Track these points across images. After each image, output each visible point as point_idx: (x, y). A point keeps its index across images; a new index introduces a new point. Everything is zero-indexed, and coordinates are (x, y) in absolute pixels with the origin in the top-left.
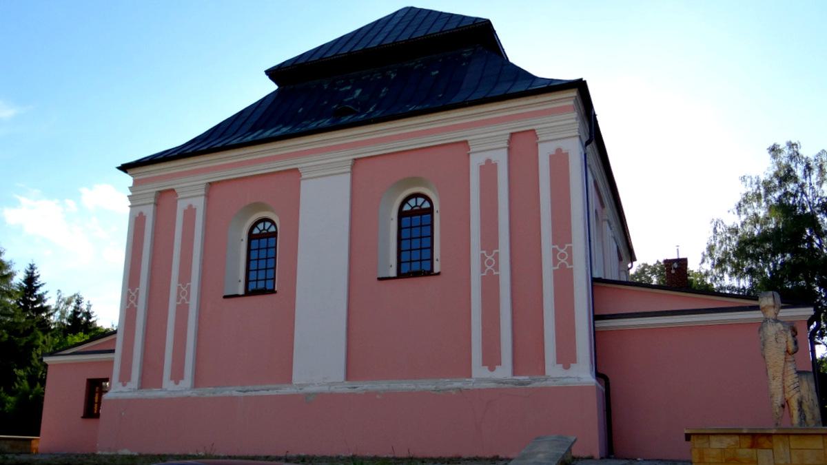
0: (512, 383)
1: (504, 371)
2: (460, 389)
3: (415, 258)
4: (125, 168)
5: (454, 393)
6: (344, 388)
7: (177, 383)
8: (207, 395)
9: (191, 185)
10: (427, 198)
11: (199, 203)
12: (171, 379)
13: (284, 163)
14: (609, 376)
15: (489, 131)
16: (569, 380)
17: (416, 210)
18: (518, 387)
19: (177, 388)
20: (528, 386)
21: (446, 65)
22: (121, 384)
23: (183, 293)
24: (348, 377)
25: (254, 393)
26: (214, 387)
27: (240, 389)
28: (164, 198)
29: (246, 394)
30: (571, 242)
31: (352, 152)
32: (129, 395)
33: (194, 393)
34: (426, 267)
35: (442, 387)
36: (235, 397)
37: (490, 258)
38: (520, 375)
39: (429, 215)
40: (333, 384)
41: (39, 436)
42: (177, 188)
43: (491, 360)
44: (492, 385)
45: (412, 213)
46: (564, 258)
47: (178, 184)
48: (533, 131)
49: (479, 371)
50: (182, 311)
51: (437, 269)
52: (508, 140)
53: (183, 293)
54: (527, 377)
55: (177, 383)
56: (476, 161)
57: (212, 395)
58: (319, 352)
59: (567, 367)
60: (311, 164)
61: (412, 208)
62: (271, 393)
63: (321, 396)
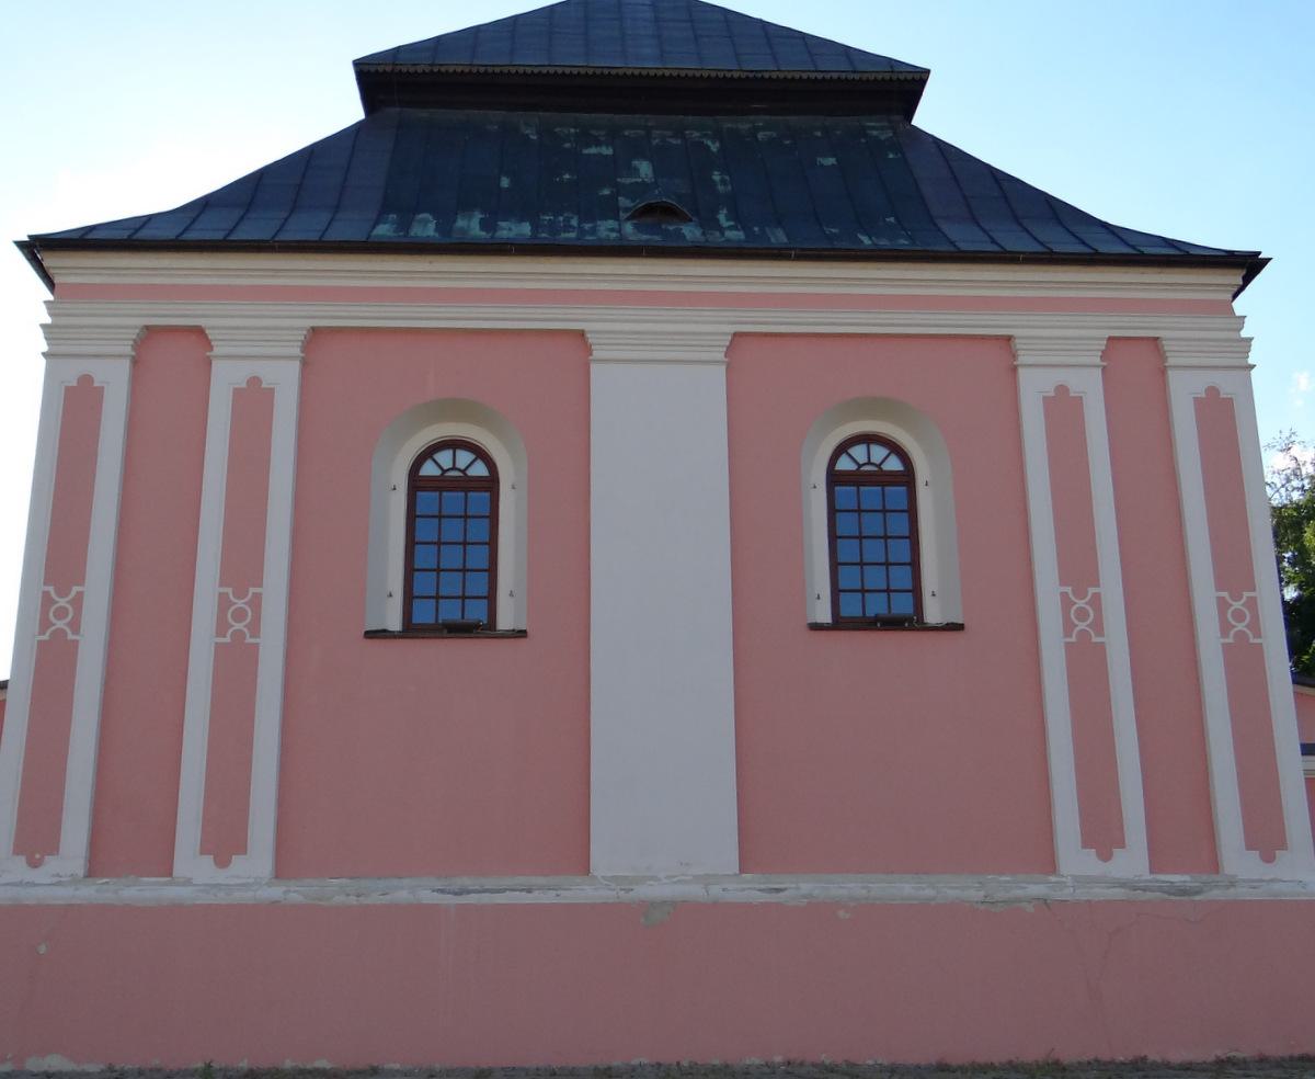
0: (1160, 889)
1: (1132, 861)
2: (1044, 902)
3: (877, 590)
4: (37, 249)
5: (1030, 908)
6: (749, 890)
8: (339, 899)
9: (261, 322)
10: (481, 454)
11: (284, 379)
12: (204, 851)
14: (231, 865)
16: (1276, 887)
17: (869, 474)
18: (1173, 898)
19: (221, 876)
20: (1197, 898)
21: (840, 157)
22: (22, 860)
24: (746, 863)
25: (486, 899)
26: (351, 878)
27: (439, 884)
28: (173, 354)
29: (472, 899)
30: (260, 585)
32: (63, 895)
33: (90, 893)
34: (476, 612)
35: (1000, 895)
37: (62, 602)
38: (1161, 871)
39: (487, 495)
40: (707, 880)
42: (213, 328)
43: (224, 841)
44: (1118, 893)
45: (441, 484)
48: (581, 334)
49: (1074, 858)
50: (236, 664)
51: (505, 621)
52: (728, 348)
54: (1186, 878)
56: (226, 379)
57: (353, 900)
58: (664, 801)
59: (1268, 858)
61: (444, 471)
62: (548, 898)
63: (681, 909)
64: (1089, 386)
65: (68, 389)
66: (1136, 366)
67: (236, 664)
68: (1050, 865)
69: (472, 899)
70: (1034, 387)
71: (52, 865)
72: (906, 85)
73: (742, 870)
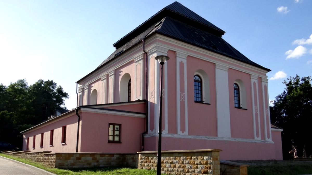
1: (186, 133)
6: (232, 140)
7: (183, 132)
13: (209, 59)
15: (170, 48)
21: (206, 36)
23: (182, 97)
29: (209, 139)
31: (230, 65)
36: (205, 140)
41: (22, 150)
43: (183, 130)
46: (183, 98)
47: (217, 63)
50: (182, 103)
53: (182, 97)
55: (183, 132)
57: (198, 138)
60: (162, 47)
64: (256, 82)
66: (260, 79)
67: (182, 103)
72: (223, 33)
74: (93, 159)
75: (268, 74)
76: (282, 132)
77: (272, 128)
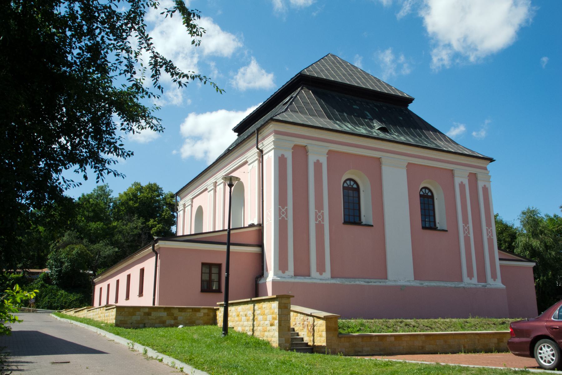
3: (352, 216)
6: (417, 284)
29: (370, 284)
40: (409, 281)
49: (466, 279)
62: (382, 284)
64: (466, 182)
65: (279, 157)
66: (473, 178)
68: (461, 281)
69: (370, 284)
70: (457, 181)
71: (287, 273)
73: (415, 279)
74: (168, 315)
75: (490, 166)
76: (535, 269)
77: (500, 259)
